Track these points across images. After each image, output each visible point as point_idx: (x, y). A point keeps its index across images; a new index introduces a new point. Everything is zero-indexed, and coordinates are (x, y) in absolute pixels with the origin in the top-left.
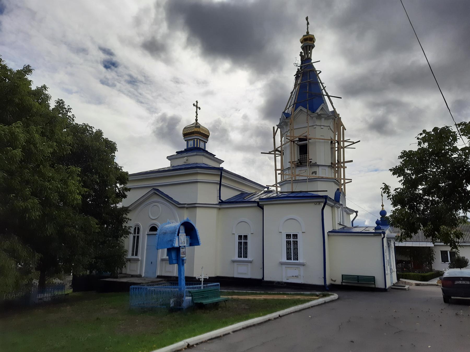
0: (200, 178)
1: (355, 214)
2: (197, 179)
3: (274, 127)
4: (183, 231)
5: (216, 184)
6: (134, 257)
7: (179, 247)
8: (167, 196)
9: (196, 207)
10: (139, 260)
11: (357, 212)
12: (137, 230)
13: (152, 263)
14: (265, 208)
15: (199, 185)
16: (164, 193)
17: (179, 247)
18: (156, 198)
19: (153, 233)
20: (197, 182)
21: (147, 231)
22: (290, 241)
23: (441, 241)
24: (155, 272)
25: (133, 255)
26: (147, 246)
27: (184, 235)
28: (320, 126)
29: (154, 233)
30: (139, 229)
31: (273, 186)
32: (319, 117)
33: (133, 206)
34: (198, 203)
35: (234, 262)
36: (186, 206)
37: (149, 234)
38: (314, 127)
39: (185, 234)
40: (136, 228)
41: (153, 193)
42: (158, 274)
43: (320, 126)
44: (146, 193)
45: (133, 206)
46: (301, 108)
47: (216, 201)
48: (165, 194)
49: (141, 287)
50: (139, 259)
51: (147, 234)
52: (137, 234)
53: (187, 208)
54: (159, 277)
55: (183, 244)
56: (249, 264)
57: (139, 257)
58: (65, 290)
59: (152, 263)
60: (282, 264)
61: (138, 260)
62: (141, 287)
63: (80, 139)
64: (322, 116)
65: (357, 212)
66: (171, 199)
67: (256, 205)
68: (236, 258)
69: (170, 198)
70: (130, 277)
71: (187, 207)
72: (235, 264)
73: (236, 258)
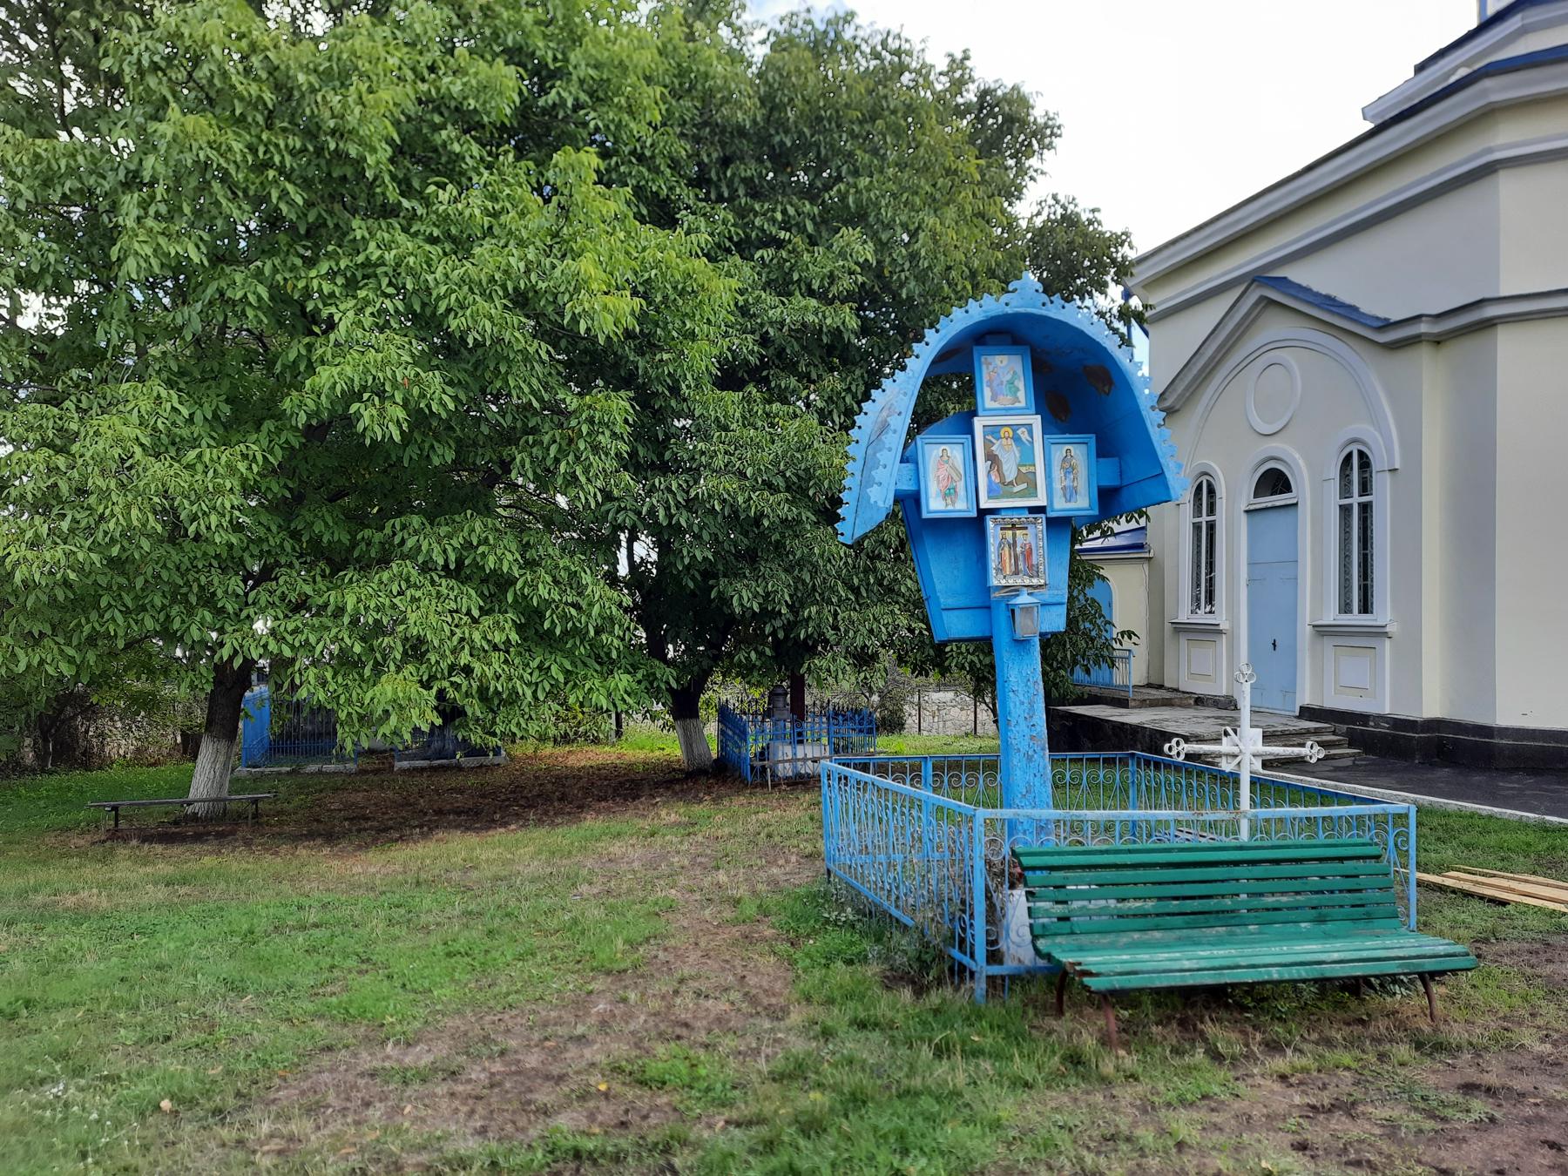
0: (1507, 138)
2: (1490, 150)
4: (1021, 395)
6: (1201, 617)
7: (974, 514)
8: (1329, 303)
9: (1489, 324)
10: (1220, 632)
12: (1205, 495)
13: (1274, 644)
15: (1507, 185)
16: (1315, 290)
17: (974, 514)
18: (1275, 328)
19: (1270, 505)
20: (1488, 170)
21: (1246, 498)
23: (41, 757)
24: (1290, 690)
26: (1252, 564)
27: (1029, 427)
29: (1278, 504)
30: (1211, 491)
33: (1180, 387)
34: (1504, 292)
36: (1423, 328)
37: (1252, 507)
39: (1036, 421)
40: (1199, 487)
41: (1256, 304)
42: (1307, 698)
44: (1227, 313)
45: (1180, 387)
48: (1317, 295)
50: (1221, 627)
51: (1247, 512)
53: (1438, 341)
54: (1307, 713)
55: (1021, 495)
57: (1221, 619)
58: (376, 772)
59: (1274, 644)
61: (1214, 631)
63: (777, 78)
66: (1350, 312)
69: (1341, 311)
70: (1187, 706)
71: (1439, 334)
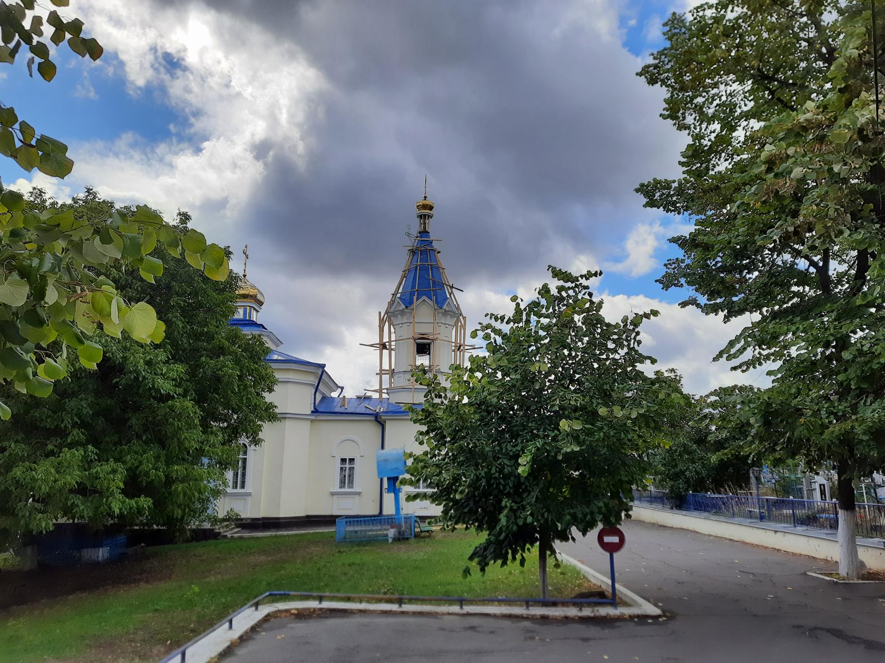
1: (339, 390)
3: (380, 313)
5: (311, 386)
9: (285, 418)
11: (342, 388)
14: (389, 426)
22: (804, 501)
25: (236, 487)
28: (445, 324)
31: (375, 391)
32: (446, 313)
35: (333, 494)
38: (439, 324)
43: (445, 324)
46: (424, 298)
47: (308, 409)
49: (350, 520)
52: (808, 498)
56: (357, 497)
60: (333, 495)
62: (350, 520)
64: (449, 313)
65: (342, 388)
67: (373, 418)
68: (337, 489)
72: (335, 497)
73: (337, 489)
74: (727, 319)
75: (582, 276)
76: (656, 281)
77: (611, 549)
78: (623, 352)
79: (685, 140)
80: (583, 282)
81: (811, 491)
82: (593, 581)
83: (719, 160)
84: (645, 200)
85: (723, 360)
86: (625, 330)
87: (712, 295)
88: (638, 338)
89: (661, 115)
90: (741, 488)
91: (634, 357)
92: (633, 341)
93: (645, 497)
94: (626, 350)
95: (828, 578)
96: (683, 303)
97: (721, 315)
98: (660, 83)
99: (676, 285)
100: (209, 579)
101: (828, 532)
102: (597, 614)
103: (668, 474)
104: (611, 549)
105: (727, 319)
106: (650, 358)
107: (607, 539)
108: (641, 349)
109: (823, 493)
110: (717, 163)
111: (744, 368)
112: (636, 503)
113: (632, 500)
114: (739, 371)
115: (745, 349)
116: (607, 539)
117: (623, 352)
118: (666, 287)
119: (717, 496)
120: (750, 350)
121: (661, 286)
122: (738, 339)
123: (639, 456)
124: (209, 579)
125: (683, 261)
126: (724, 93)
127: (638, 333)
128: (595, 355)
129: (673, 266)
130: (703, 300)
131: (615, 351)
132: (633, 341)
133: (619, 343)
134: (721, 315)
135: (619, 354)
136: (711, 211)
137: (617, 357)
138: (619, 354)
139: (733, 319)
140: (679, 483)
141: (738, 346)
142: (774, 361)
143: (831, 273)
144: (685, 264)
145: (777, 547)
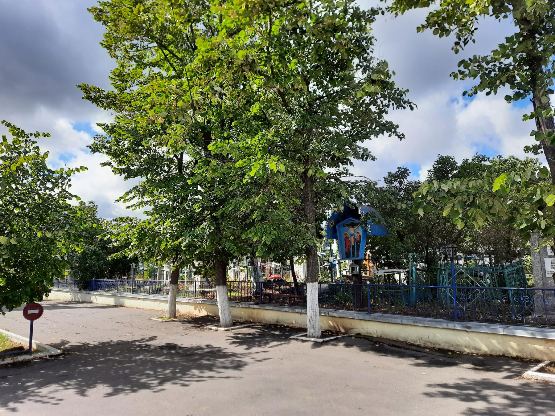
74: (126, 178)
75: (31, 134)
76: (88, 146)
77: (32, 318)
78: (57, 190)
79: (114, 65)
80: (33, 138)
81: (161, 275)
82: (15, 341)
83: (133, 83)
84: (84, 95)
85: (121, 202)
86: (61, 177)
87: (121, 163)
88: (69, 183)
89: (101, 44)
90: (125, 275)
91: (65, 194)
92: (65, 184)
93: (62, 284)
94: (60, 190)
95: (160, 320)
96: (103, 164)
97: (124, 175)
98: (102, 22)
99: (100, 152)
100: (200, 362)
101: (165, 296)
102: (16, 361)
103: (80, 268)
104: (32, 318)
105: (126, 178)
106: (76, 196)
107: (30, 312)
108: (69, 190)
109: (167, 276)
110: (156, 77)
111: (134, 207)
112: (55, 288)
113: (52, 285)
114: (131, 209)
115: (134, 197)
116: (30, 312)
117: (57, 190)
118: (94, 151)
119: (110, 280)
120: (136, 198)
121: (91, 150)
122: (131, 191)
123: (61, 257)
124: (200, 362)
125: (105, 138)
126: (140, 46)
127: (70, 180)
128: (319, 132)
129: (99, 139)
130: (115, 165)
131: (52, 189)
132: (65, 184)
133: (55, 185)
134: (124, 175)
135: (54, 192)
136: (126, 111)
137: (53, 193)
138: (54, 192)
139: (130, 179)
140: (87, 274)
141: (131, 195)
142: (150, 205)
143: (184, 162)
144: (107, 140)
145: (139, 307)
